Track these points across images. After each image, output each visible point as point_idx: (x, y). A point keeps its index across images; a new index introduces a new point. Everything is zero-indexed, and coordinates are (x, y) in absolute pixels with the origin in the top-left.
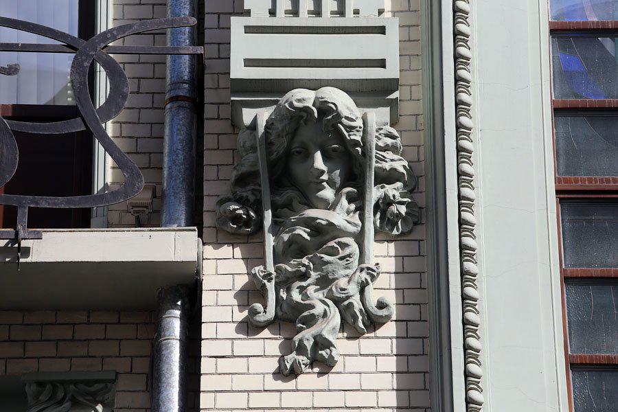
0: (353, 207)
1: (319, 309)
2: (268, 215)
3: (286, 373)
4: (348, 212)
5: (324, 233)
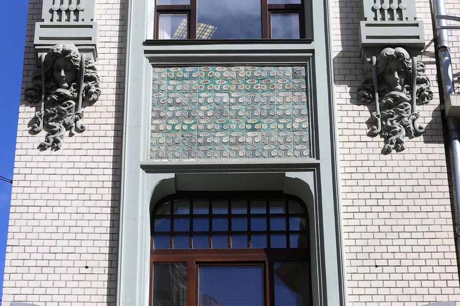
0: (408, 92)
1: (398, 129)
2: (377, 95)
3: (386, 152)
4: (407, 94)
5: (63, 98)
